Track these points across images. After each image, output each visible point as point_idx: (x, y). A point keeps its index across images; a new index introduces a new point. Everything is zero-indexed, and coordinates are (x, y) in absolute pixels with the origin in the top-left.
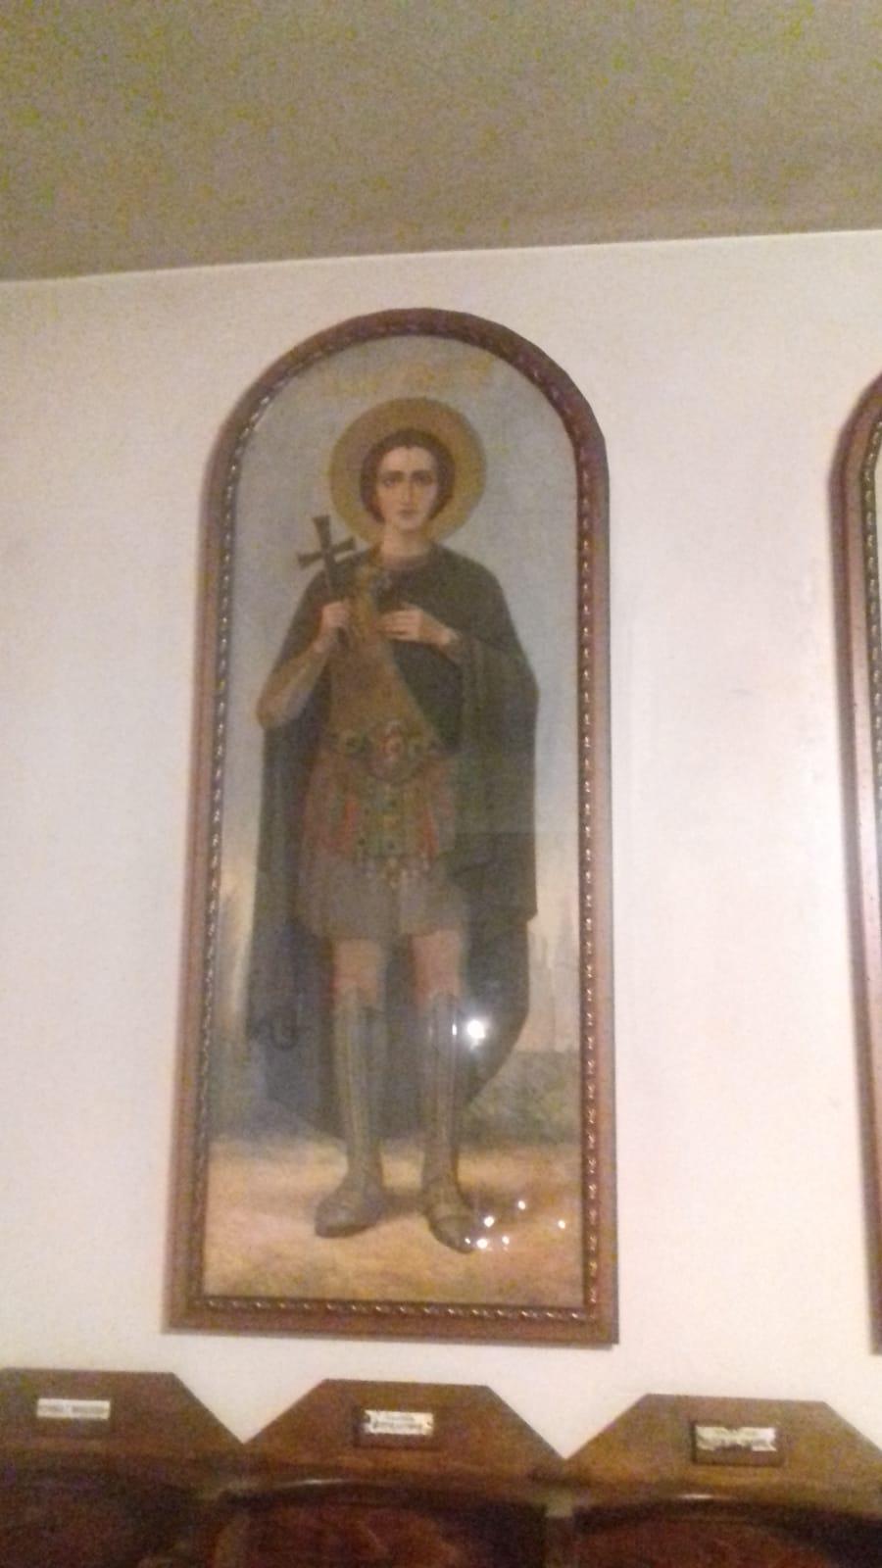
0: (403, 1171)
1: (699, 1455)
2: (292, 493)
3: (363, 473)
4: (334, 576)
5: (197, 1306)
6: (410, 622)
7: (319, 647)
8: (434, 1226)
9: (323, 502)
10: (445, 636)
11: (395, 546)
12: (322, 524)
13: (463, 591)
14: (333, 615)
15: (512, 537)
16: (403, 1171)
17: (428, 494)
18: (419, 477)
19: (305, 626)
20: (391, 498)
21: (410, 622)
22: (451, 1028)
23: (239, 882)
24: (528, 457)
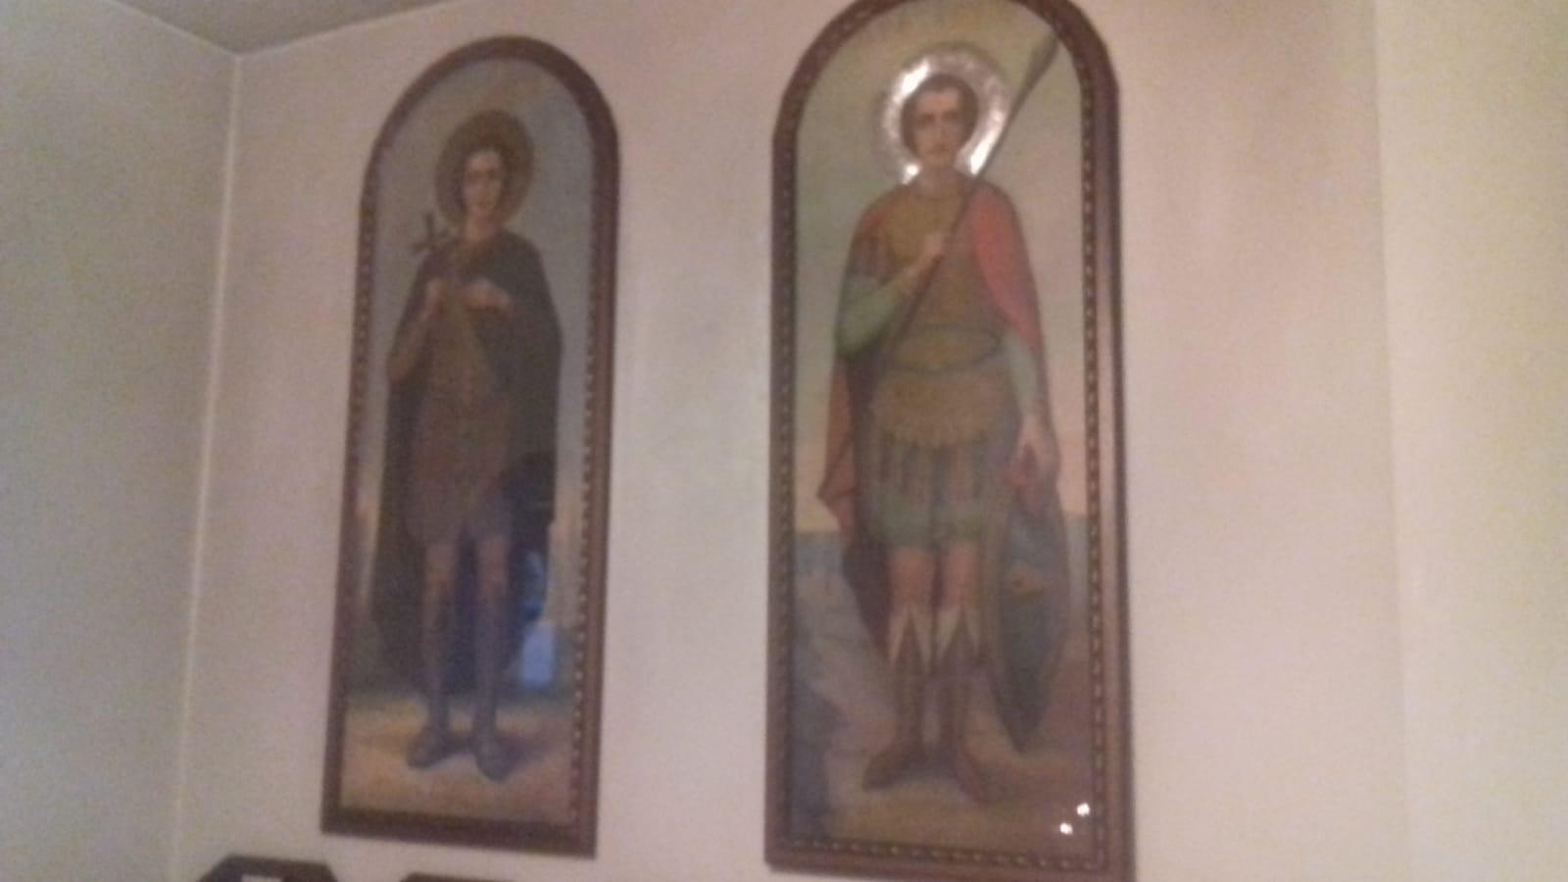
0: (461, 721)
1: (346, 801)
2: (413, 196)
3: (452, 182)
4: (435, 261)
5: (343, 816)
6: (482, 291)
7: (425, 315)
8: (480, 763)
9: (430, 201)
10: (504, 300)
11: (475, 232)
12: (429, 220)
13: (513, 261)
14: (433, 289)
15: (551, 223)
16: (461, 721)
17: (496, 185)
18: (491, 174)
19: (416, 302)
20: (473, 192)
21: (482, 291)
22: (909, 65)
23: (370, 504)
24: (563, 145)
